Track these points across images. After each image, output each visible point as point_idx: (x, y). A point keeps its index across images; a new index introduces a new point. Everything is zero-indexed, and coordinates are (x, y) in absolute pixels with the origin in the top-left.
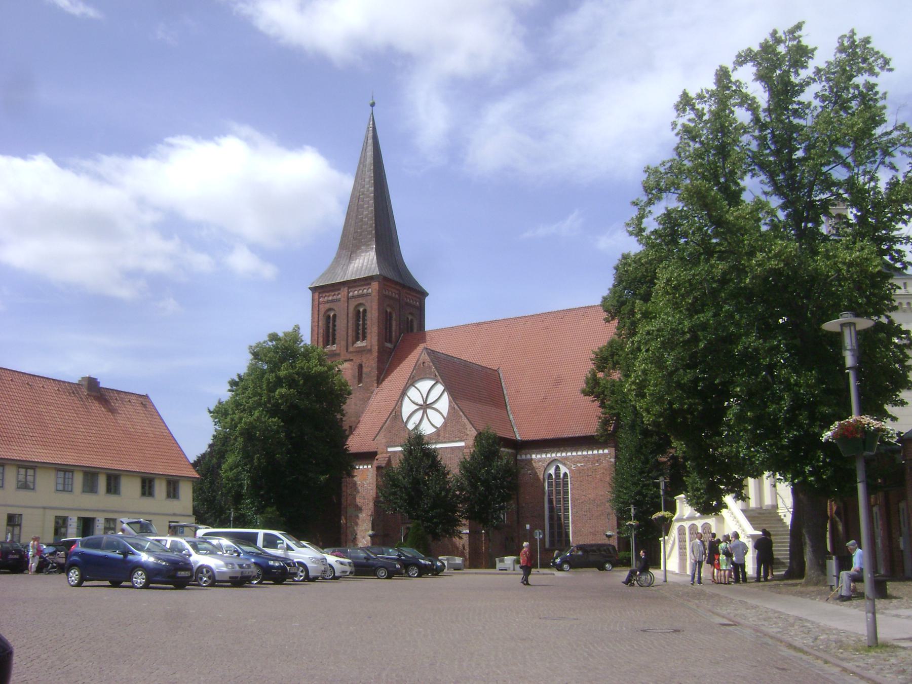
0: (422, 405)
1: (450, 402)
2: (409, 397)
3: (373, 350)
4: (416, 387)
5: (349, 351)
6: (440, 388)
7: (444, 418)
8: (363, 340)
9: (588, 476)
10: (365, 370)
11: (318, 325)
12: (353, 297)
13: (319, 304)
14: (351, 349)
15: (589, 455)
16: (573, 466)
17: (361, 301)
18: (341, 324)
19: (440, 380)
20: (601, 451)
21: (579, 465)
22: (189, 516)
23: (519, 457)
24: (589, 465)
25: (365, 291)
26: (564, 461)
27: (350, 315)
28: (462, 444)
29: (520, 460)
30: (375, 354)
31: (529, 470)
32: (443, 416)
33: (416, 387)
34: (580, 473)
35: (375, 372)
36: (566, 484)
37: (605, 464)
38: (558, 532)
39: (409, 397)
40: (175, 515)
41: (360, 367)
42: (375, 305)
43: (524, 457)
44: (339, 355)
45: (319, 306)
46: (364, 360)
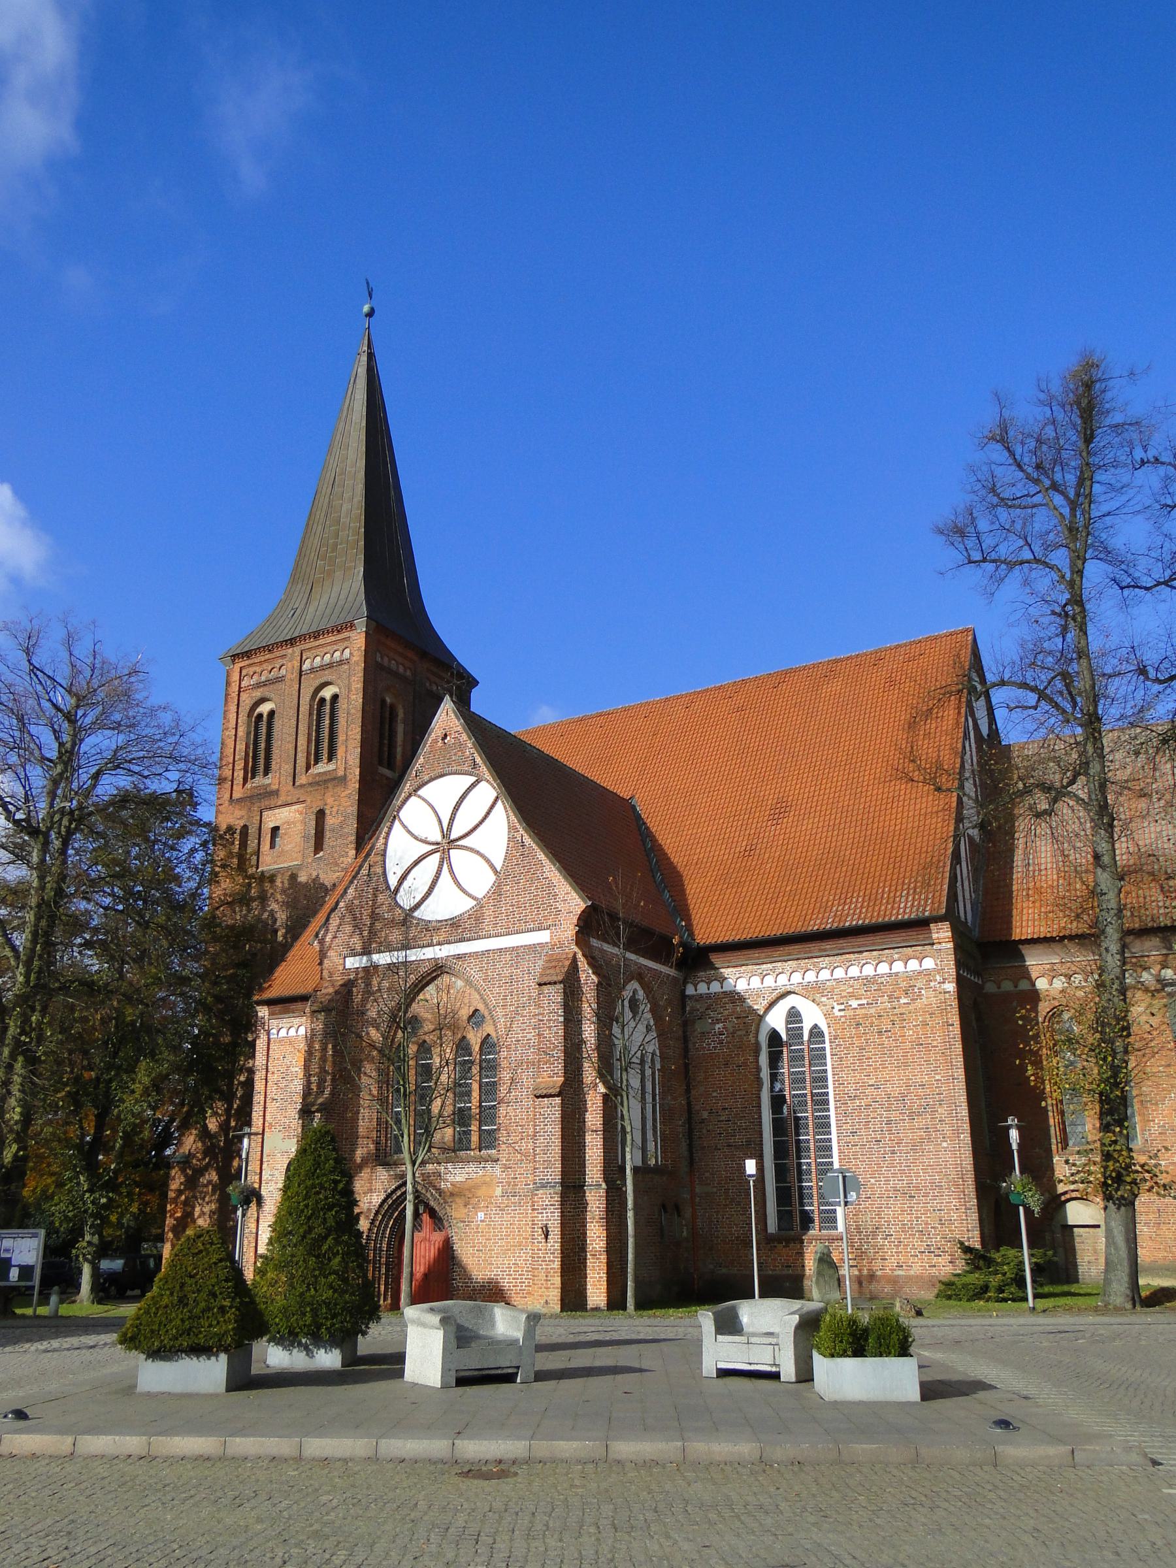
0: (438, 844)
1: (512, 828)
2: (405, 827)
3: (349, 777)
4: (419, 797)
5: (297, 784)
6: (486, 792)
7: (496, 872)
8: (330, 759)
10: (330, 821)
11: (236, 735)
12: (312, 670)
13: (239, 692)
14: (302, 779)
15: (882, 976)
16: (837, 1007)
17: (327, 676)
18: (283, 730)
19: (487, 775)
23: (690, 990)
24: (884, 1003)
26: (813, 991)
27: (304, 708)
28: (543, 937)
29: (691, 997)
30: (354, 785)
31: (718, 1021)
32: (473, 786)
33: (419, 797)
35: (352, 826)
36: (818, 1057)
37: (928, 998)
39: (405, 827)
41: (321, 815)
42: (357, 684)
43: (702, 988)
44: (276, 793)
45: (239, 695)
46: (330, 801)
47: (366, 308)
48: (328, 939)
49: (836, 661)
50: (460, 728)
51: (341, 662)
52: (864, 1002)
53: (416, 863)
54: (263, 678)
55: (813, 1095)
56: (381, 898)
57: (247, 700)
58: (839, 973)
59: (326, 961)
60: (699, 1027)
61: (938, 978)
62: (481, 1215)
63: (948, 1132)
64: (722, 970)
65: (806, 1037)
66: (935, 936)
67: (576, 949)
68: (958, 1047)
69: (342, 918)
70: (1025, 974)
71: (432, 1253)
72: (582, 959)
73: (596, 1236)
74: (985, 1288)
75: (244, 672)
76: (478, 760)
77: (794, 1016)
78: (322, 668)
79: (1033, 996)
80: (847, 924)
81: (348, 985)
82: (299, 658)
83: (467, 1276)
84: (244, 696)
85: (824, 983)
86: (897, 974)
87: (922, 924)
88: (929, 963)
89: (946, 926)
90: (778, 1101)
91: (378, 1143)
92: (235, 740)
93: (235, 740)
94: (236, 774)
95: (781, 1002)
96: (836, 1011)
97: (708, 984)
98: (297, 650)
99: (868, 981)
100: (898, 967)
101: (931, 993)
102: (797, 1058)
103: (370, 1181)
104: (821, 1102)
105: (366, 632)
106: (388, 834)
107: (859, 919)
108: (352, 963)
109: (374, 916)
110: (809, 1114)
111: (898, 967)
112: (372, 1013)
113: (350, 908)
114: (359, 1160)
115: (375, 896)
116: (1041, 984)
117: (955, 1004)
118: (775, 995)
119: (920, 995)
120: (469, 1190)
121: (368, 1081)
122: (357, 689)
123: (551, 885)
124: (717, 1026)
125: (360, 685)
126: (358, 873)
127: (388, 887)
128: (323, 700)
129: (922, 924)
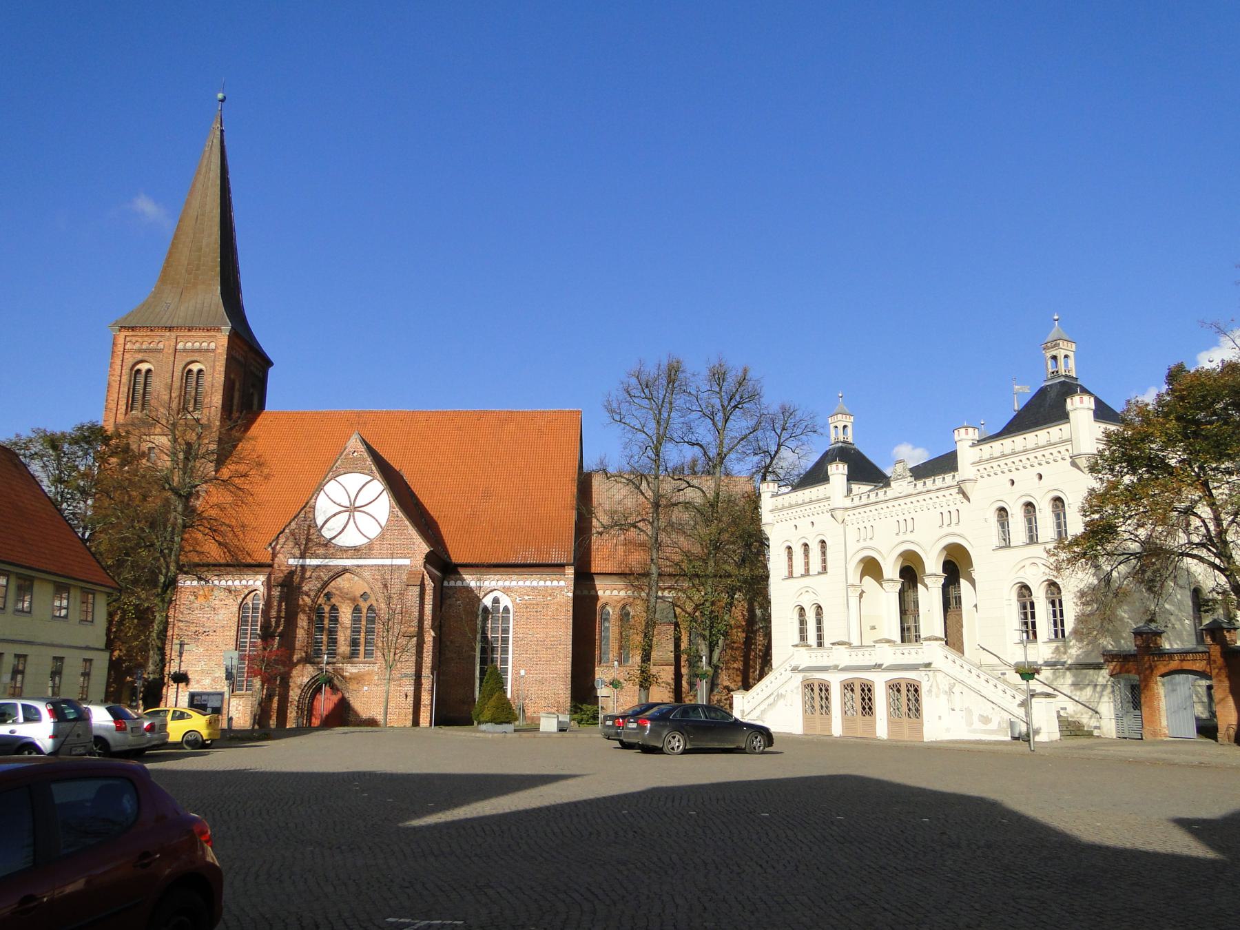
7: (381, 527)
9: (537, 612)
12: (185, 350)
13: (124, 352)
16: (518, 599)
17: (196, 357)
20: (555, 583)
21: (526, 598)
22: (102, 650)
23: (446, 584)
24: (540, 599)
25: (205, 344)
26: (506, 590)
28: (406, 562)
29: (447, 587)
34: (527, 607)
36: (506, 620)
37: (560, 598)
38: (1031, 612)
40: (87, 648)
43: (452, 583)
45: (123, 354)
47: (220, 96)
48: (278, 547)
49: (511, 412)
50: (363, 450)
51: (208, 351)
52: (531, 597)
53: (335, 515)
54: (144, 347)
55: (502, 637)
56: (312, 531)
57: (130, 360)
58: (521, 583)
59: (276, 559)
60: (448, 602)
61: (566, 590)
62: (366, 688)
63: (562, 656)
64: (471, 581)
65: (501, 611)
66: (566, 571)
67: (424, 570)
68: (571, 621)
69: (287, 539)
70: (594, 587)
71: (331, 705)
72: (427, 575)
73: (426, 698)
74: (582, 720)
75: (128, 339)
76: (374, 469)
77: (496, 601)
78: (193, 351)
79: (596, 598)
80: (528, 562)
81: (292, 573)
82: (175, 340)
83: (356, 713)
84: (127, 356)
85: (513, 587)
86: (547, 586)
87: (562, 566)
88: (562, 583)
89: (572, 568)
90: (485, 638)
91: (306, 653)
92: (120, 384)
93: (120, 384)
94: (119, 407)
95: (491, 593)
96: (517, 600)
97: (456, 582)
98: (174, 334)
99: (534, 588)
100: (548, 583)
101: (562, 596)
102: (495, 620)
103: (302, 670)
104: (505, 640)
105: (229, 336)
106: (317, 497)
107: (534, 559)
108: (292, 561)
109: (308, 540)
110: (250, 615)
111: (548, 583)
112: (305, 588)
113: (292, 533)
114: (295, 661)
115: (309, 529)
116: (600, 593)
117: (572, 602)
118: (488, 590)
119: (556, 597)
120: (360, 676)
121: (303, 621)
122: (220, 371)
123: (412, 538)
124: (458, 602)
125: (223, 369)
126: (298, 515)
127: (317, 526)
128: (190, 371)
129: (562, 566)
